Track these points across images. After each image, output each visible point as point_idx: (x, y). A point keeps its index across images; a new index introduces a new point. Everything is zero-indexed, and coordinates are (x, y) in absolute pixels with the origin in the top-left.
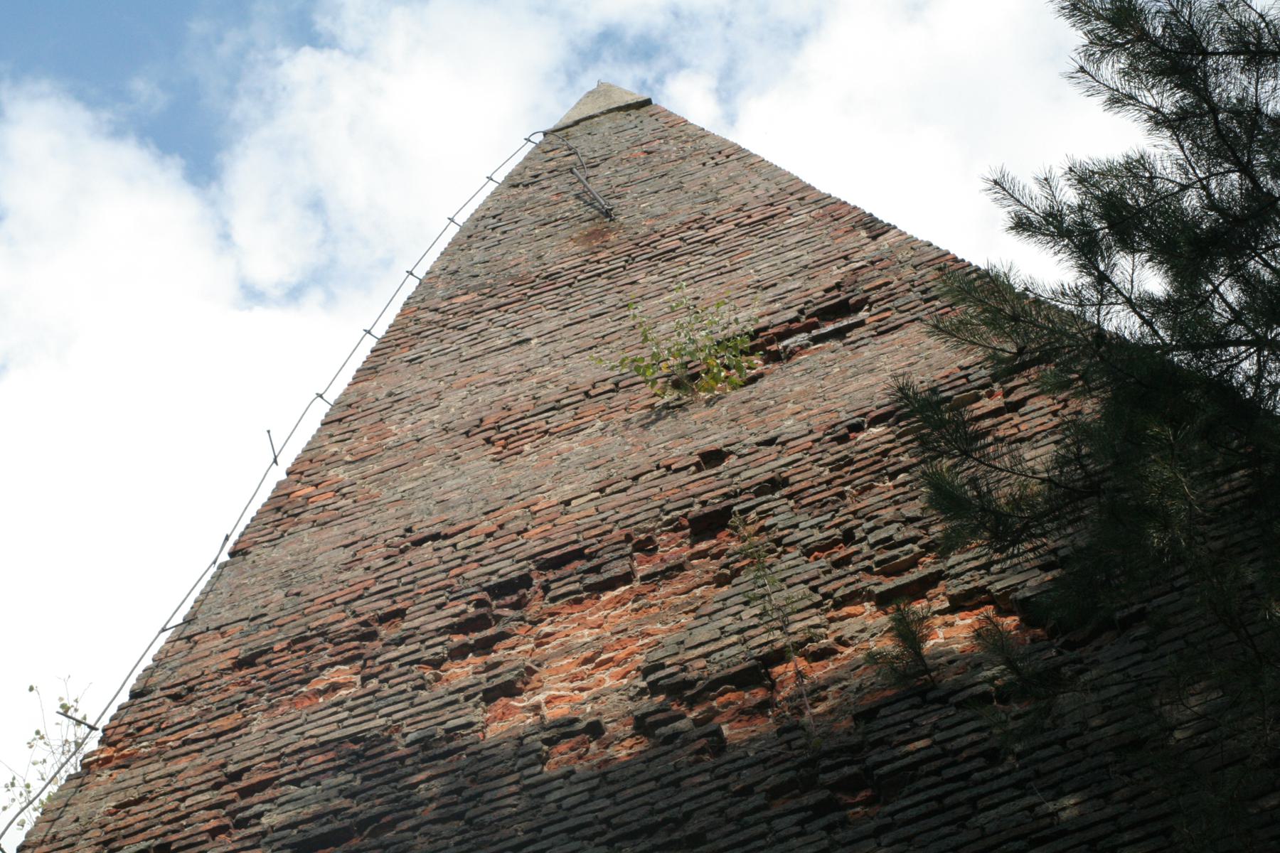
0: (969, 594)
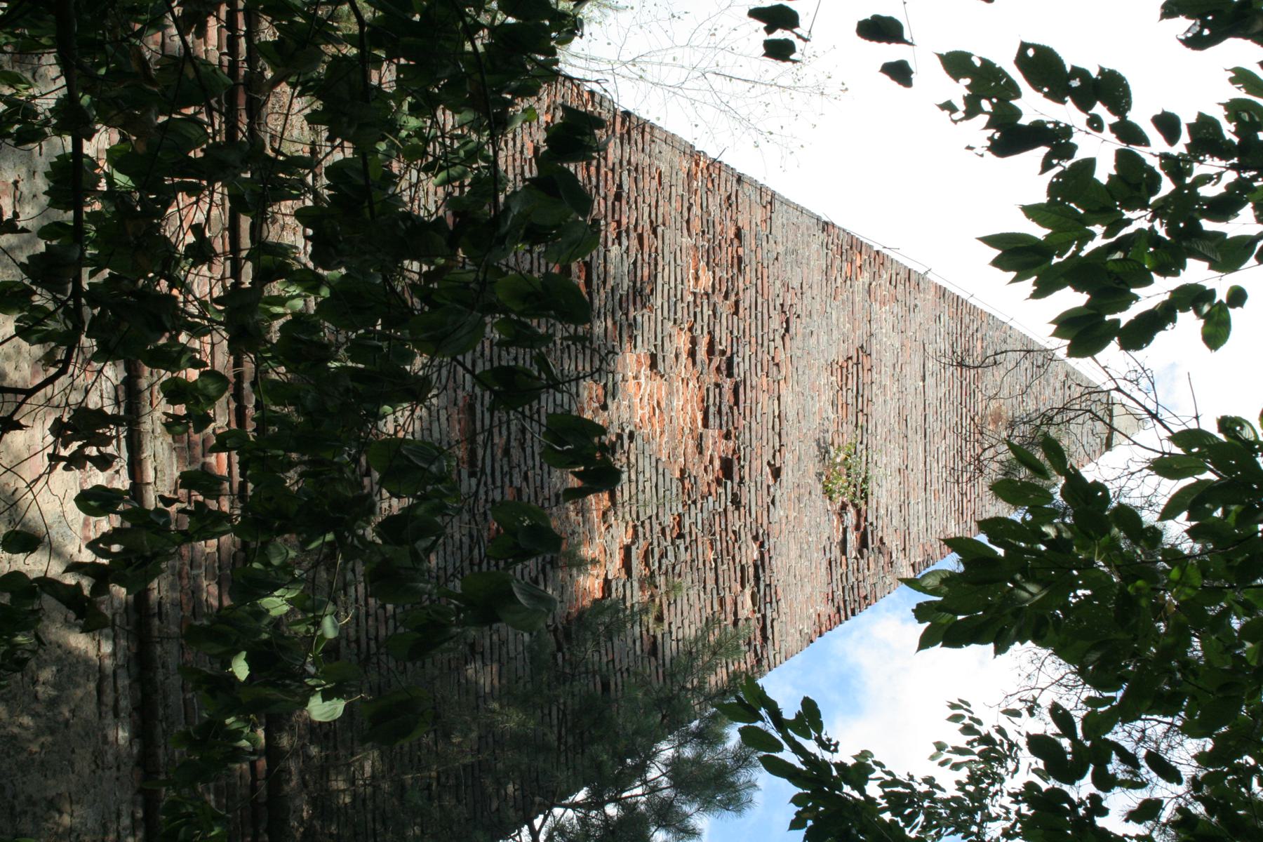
0: (610, 589)
